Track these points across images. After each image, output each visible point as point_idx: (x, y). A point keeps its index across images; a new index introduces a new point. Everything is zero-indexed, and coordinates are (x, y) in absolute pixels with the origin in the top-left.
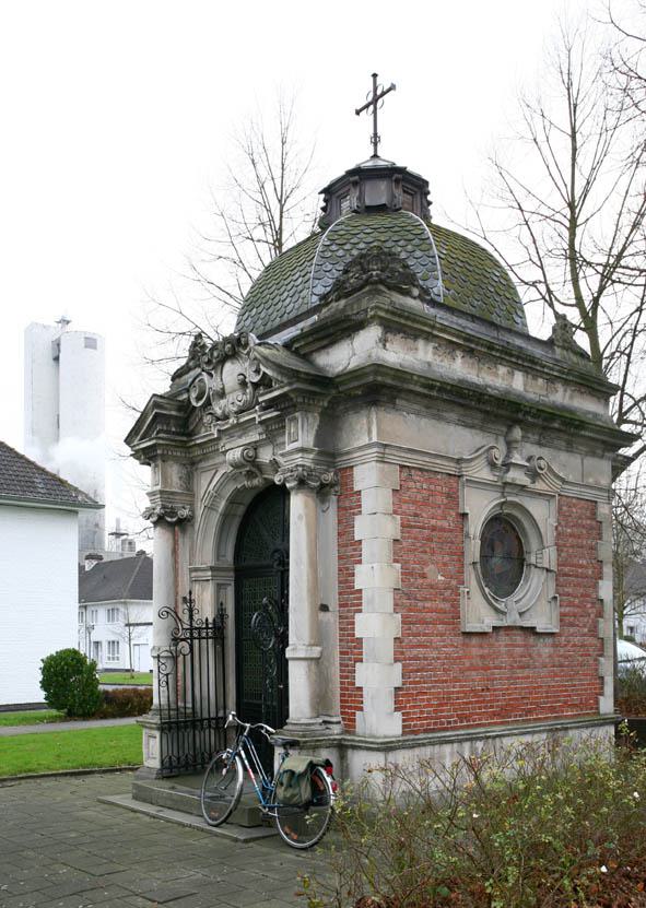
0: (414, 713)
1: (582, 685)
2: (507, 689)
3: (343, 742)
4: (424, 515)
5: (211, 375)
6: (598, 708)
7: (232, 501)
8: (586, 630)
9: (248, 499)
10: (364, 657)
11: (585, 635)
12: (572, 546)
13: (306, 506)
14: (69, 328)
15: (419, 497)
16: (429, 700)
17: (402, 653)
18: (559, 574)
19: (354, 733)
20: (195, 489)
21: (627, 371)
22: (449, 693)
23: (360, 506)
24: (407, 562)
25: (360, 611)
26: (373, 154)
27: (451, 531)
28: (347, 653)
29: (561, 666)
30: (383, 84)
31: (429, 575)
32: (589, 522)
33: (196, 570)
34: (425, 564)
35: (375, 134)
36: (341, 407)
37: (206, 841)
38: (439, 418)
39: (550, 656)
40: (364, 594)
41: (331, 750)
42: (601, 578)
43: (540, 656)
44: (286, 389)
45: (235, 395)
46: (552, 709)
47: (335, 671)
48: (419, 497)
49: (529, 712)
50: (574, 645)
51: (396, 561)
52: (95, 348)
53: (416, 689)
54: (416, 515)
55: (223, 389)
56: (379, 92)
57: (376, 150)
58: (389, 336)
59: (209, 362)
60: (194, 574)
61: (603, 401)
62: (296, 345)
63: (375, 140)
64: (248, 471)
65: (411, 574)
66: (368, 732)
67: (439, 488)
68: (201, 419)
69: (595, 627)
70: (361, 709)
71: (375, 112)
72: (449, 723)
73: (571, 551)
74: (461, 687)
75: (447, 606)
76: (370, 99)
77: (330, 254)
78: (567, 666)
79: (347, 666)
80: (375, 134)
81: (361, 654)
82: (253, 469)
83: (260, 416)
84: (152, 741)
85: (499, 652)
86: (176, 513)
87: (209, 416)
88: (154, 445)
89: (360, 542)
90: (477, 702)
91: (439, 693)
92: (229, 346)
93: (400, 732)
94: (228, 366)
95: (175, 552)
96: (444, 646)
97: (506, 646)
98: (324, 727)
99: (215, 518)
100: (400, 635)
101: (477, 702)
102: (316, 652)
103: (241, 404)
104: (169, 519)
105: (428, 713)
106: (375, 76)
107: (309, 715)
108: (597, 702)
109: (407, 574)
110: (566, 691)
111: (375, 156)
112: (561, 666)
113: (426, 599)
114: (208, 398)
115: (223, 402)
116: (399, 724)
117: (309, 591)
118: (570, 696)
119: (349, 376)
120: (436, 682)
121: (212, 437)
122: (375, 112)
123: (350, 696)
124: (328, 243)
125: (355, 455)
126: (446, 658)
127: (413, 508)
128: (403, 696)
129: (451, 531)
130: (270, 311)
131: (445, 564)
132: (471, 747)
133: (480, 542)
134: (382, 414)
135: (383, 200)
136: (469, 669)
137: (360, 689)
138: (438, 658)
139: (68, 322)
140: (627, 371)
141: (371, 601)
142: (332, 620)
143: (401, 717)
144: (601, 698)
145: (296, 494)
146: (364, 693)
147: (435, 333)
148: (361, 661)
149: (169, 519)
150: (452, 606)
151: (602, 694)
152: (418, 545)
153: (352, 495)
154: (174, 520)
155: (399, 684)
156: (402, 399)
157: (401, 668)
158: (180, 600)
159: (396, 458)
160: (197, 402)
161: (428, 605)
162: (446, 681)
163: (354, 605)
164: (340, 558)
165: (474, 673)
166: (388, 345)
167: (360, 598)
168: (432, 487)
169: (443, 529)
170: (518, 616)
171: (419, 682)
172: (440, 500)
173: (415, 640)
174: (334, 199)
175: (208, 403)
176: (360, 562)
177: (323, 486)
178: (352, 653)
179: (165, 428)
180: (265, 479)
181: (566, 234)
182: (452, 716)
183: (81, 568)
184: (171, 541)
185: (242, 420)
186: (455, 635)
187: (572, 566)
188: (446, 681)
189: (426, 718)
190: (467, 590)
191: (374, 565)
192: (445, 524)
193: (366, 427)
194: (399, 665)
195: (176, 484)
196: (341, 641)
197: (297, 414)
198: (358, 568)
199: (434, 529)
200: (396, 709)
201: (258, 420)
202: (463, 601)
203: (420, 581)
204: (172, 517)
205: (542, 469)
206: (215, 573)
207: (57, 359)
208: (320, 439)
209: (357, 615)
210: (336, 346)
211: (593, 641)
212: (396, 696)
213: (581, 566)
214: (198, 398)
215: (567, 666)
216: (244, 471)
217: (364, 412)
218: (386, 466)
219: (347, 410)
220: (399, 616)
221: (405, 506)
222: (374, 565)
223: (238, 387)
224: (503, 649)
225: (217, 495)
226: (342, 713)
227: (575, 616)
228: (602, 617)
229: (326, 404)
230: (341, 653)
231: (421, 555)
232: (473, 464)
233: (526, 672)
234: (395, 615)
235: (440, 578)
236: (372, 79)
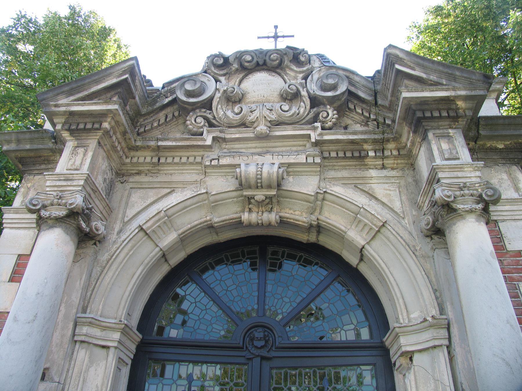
88: (102, 115)
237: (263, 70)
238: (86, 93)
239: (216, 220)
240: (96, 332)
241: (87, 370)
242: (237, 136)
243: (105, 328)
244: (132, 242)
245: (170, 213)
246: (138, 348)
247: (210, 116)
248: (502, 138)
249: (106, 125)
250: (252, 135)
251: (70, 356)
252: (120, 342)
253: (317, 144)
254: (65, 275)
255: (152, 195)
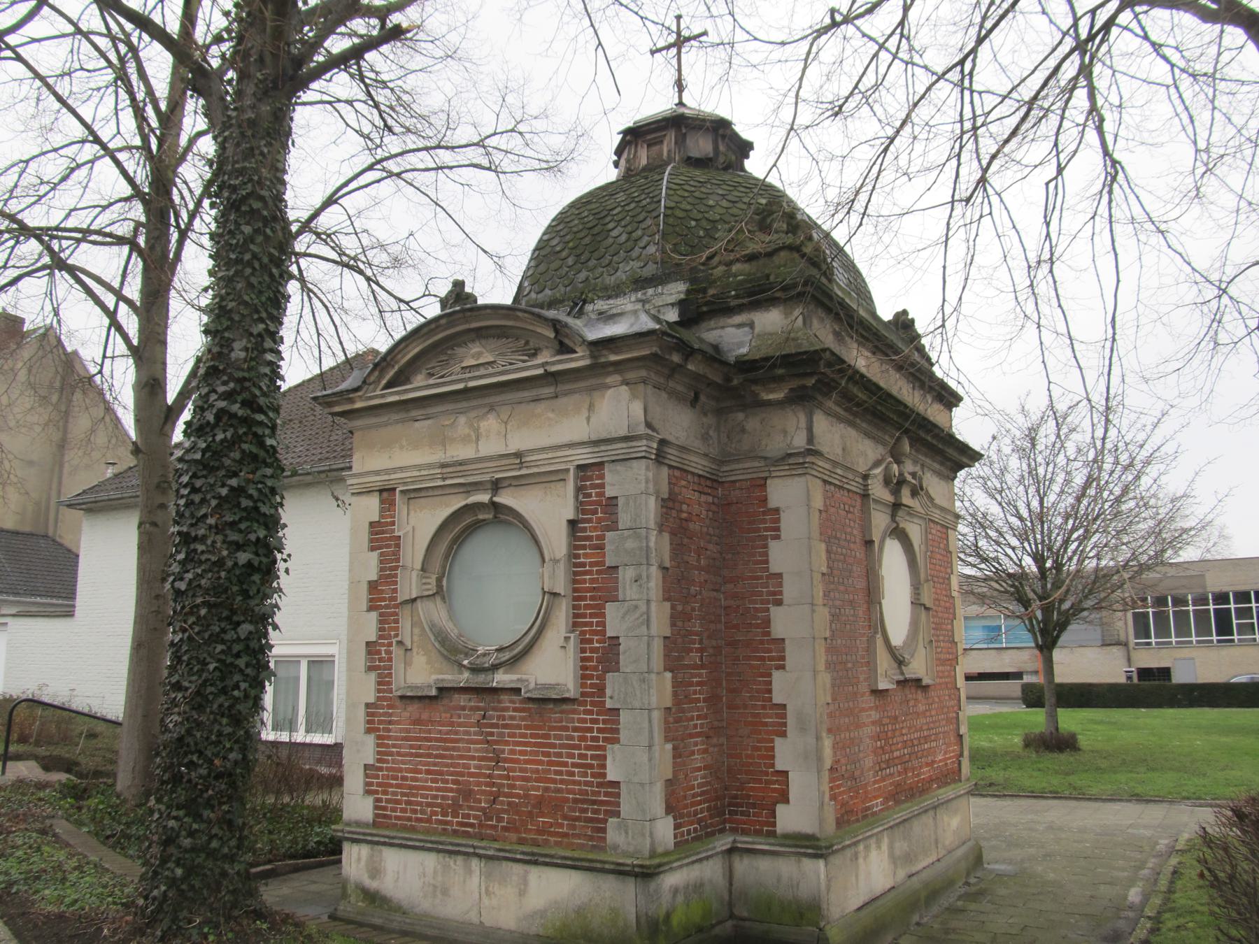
21: (1057, 295)
26: (677, 101)
57: (680, 97)
63: (680, 85)
93: (768, 482)
111: (681, 104)
116: (776, 686)
132: (372, 856)
140: (1057, 295)
143: (770, 565)
157: (344, 816)
181: (913, 115)
209: (372, 700)
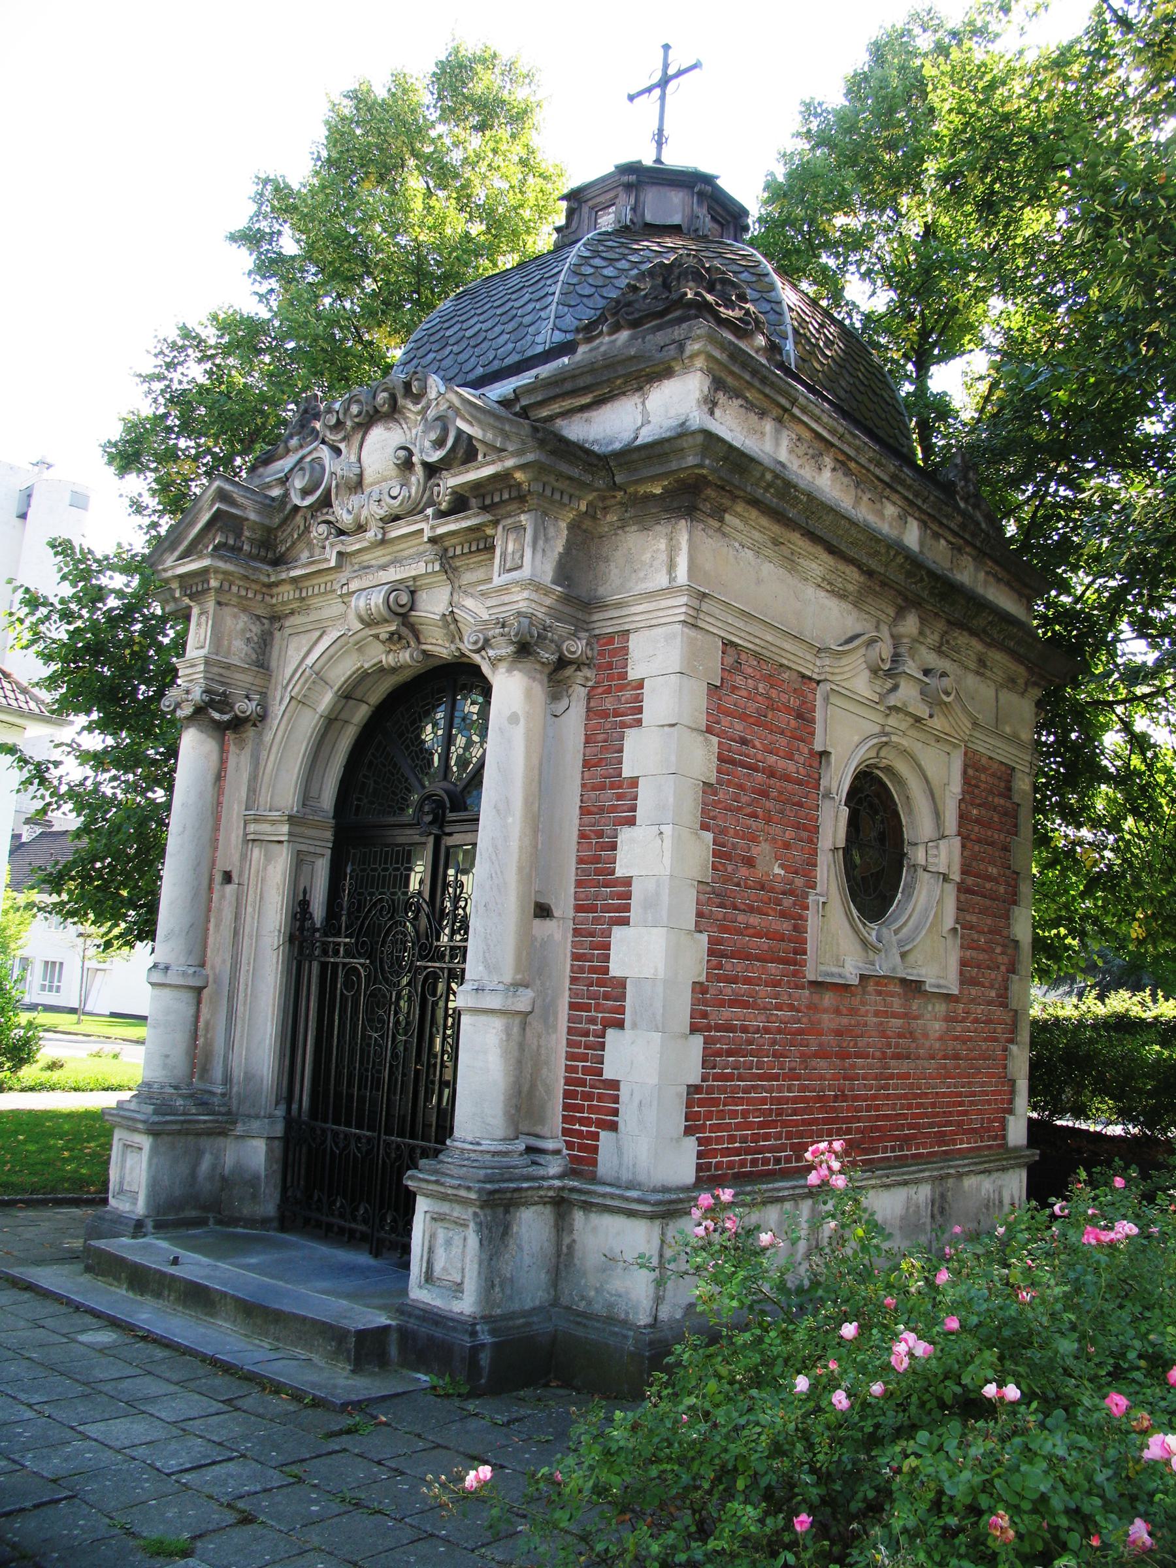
0: (719, 1140)
1: (985, 1093)
2: (875, 1097)
3: (565, 1194)
4: (757, 743)
5: (338, 452)
6: (1004, 1137)
7: (348, 695)
8: (993, 994)
9: (376, 695)
10: (628, 1017)
11: (989, 1003)
12: (979, 841)
13: (528, 694)
14: (47, 474)
15: (752, 707)
16: (745, 1113)
17: (705, 1015)
18: (962, 889)
19: (593, 1178)
20: (273, 664)
22: (779, 1101)
23: (640, 710)
24: (724, 831)
25: (625, 922)
27: (799, 783)
28: (586, 1008)
29: (956, 1057)
30: (677, 61)
31: (759, 862)
32: (1002, 801)
33: (257, 820)
34: (754, 839)
35: (661, 131)
36: (612, 518)
37: (218, 1381)
38: (790, 563)
39: (940, 1039)
40: (636, 889)
41: (540, 1208)
42: (1015, 903)
43: (926, 1036)
44: (510, 463)
45: (385, 486)
46: (941, 1139)
47: (558, 1044)
48: (752, 707)
49: (906, 1141)
50: (976, 1021)
51: (705, 827)
52: (85, 508)
53: (722, 1090)
54: (744, 742)
55: (361, 476)
56: (671, 71)
58: (721, 397)
59: (339, 424)
60: (252, 828)
61: (1024, 601)
62: (524, 402)
63: (660, 139)
64: (392, 634)
65: (727, 856)
66: (625, 1176)
67: (784, 698)
68: (307, 529)
69: (1006, 989)
70: (613, 1127)
71: (663, 98)
72: (777, 1161)
73: (977, 848)
74: (803, 1088)
75: (785, 926)
76: (657, 77)
77: (591, 270)
78: (966, 1058)
79: (586, 1034)
80: (661, 131)
81: (622, 1010)
82: (405, 631)
83: (433, 528)
84: (131, 1159)
85: (865, 1025)
86: (232, 708)
87: (323, 528)
88: (205, 571)
89: (634, 782)
90: (826, 1121)
91: (763, 1101)
92: (385, 395)
94: (377, 434)
95: (220, 777)
96: (779, 1007)
97: (877, 1014)
98: (526, 1159)
99: (308, 723)
100: (703, 978)
101: (826, 1121)
102: (523, 1001)
103: (396, 503)
104: (216, 716)
105: (744, 1139)
106: (666, 47)
107: (500, 1133)
108: (1004, 1128)
109: (721, 854)
110: (961, 1104)
112: (956, 1057)
113: (751, 910)
114: (328, 491)
115: (355, 500)
117: (520, 869)
118: (965, 1113)
119: (643, 454)
120: (761, 1077)
121: (325, 566)
122: (663, 98)
123: (588, 1097)
124: (587, 254)
125: (634, 610)
126: (779, 1031)
127: (739, 728)
128: (701, 1102)
129: (799, 783)
130: (463, 357)
131: (787, 846)
133: (845, 812)
134: (699, 534)
135: (676, 220)
136: (816, 1055)
137: (615, 1084)
138: (767, 1030)
139: (49, 466)
141: (651, 904)
142: (558, 936)
144: (1011, 1118)
145: (509, 671)
146: (624, 1093)
147: (796, 411)
148: (620, 1025)
149: (216, 716)
150: (796, 928)
151: (1011, 1111)
152: (744, 799)
153: (622, 688)
154: (226, 717)
155: (695, 1079)
156: (738, 515)
158: (218, 878)
159: (720, 625)
160: (303, 499)
161: (754, 920)
162: (776, 1077)
163: (608, 909)
164: (584, 811)
165: (822, 1063)
166: (718, 412)
167: (628, 896)
168: (774, 694)
169: (787, 778)
170: (898, 959)
171: (729, 1078)
172: (785, 720)
173: (729, 990)
174: (585, 209)
175: (326, 502)
176: (631, 822)
177: (562, 663)
178: (598, 1008)
179: (231, 542)
180: (424, 652)
182: (782, 1148)
183: (16, 837)
184: (215, 757)
185: (393, 534)
186: (797, 987)
187: (977, 876)
188: (776, 1077)
189: (737, 1151)
190: (822, 899)
191: (663, 828)
192: (791, 767)
193: (664, 557)
194: (698, 1041)
195: (239, 650)
196: (573, 980)
197: (523, 517)
198: (625, 835)
199: (771, 773)
200: (688, 1131)
201: (427, 534)
202: (812, 921)
203: (743, 871)
204: (222, 712)
205: (948, 694)
206: (298, 830)
207: (23, 516)
208: (566, 572)
210: (609, 405)
211: (998, 1012)
212: (689, 1104)
213: (989, 878)
214: (305, 493)
215: (966, 1058)
216: (384, 631)
217: (662, 529)
218: (699, 636)
219: (623, 525)
220: (704, 938)
221: (726, 720)
222: (663, 828)
223: (393, 472)
224: (872, 1020)
225: (319, 677)
226: (565, 1132)
227: (978, 967)
228: (1014, 972)
229: (583, 508)
230: (573, 1006)
231: (751, 821)
232: (844, 662)
233: (904, 1066)
234: (697, 935)
235: (777, 870)
236: (662, 51)
237: (378, 420)
238: (186, 543)
239: (366, 666)
240: (265, 827)
241: (265, 869)
242: (357, 546)
243: (274, 822)
244: (287, 715)
245: (317, 668)
246: (336, 835)
247: (331, 518)
248: (653, 479)
249: (214, 583)
250: (365, 544)
251: (244, 857)
252: (290, 834)
253: (433, 540)
254: (210, 777)
255: (305, 641)
